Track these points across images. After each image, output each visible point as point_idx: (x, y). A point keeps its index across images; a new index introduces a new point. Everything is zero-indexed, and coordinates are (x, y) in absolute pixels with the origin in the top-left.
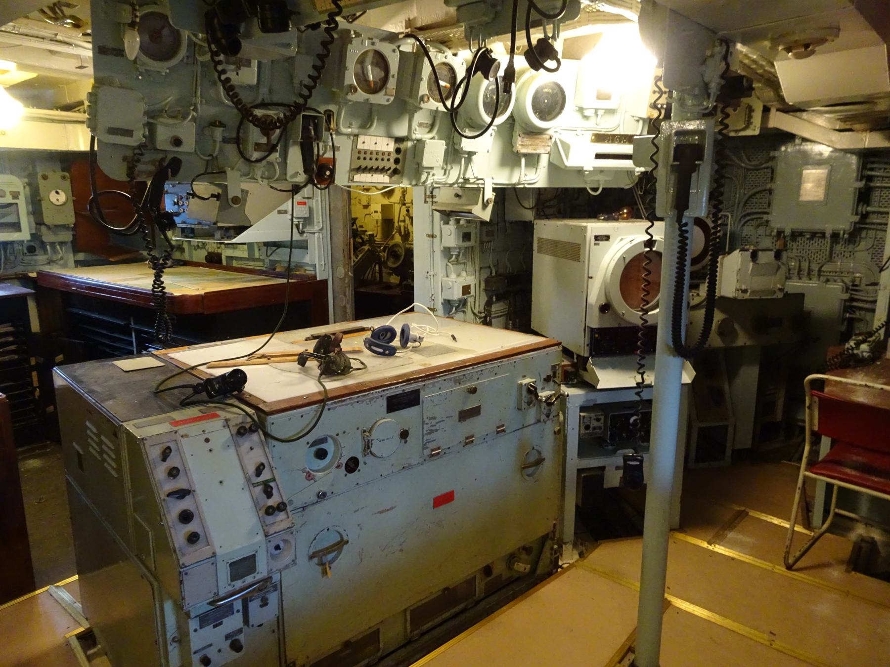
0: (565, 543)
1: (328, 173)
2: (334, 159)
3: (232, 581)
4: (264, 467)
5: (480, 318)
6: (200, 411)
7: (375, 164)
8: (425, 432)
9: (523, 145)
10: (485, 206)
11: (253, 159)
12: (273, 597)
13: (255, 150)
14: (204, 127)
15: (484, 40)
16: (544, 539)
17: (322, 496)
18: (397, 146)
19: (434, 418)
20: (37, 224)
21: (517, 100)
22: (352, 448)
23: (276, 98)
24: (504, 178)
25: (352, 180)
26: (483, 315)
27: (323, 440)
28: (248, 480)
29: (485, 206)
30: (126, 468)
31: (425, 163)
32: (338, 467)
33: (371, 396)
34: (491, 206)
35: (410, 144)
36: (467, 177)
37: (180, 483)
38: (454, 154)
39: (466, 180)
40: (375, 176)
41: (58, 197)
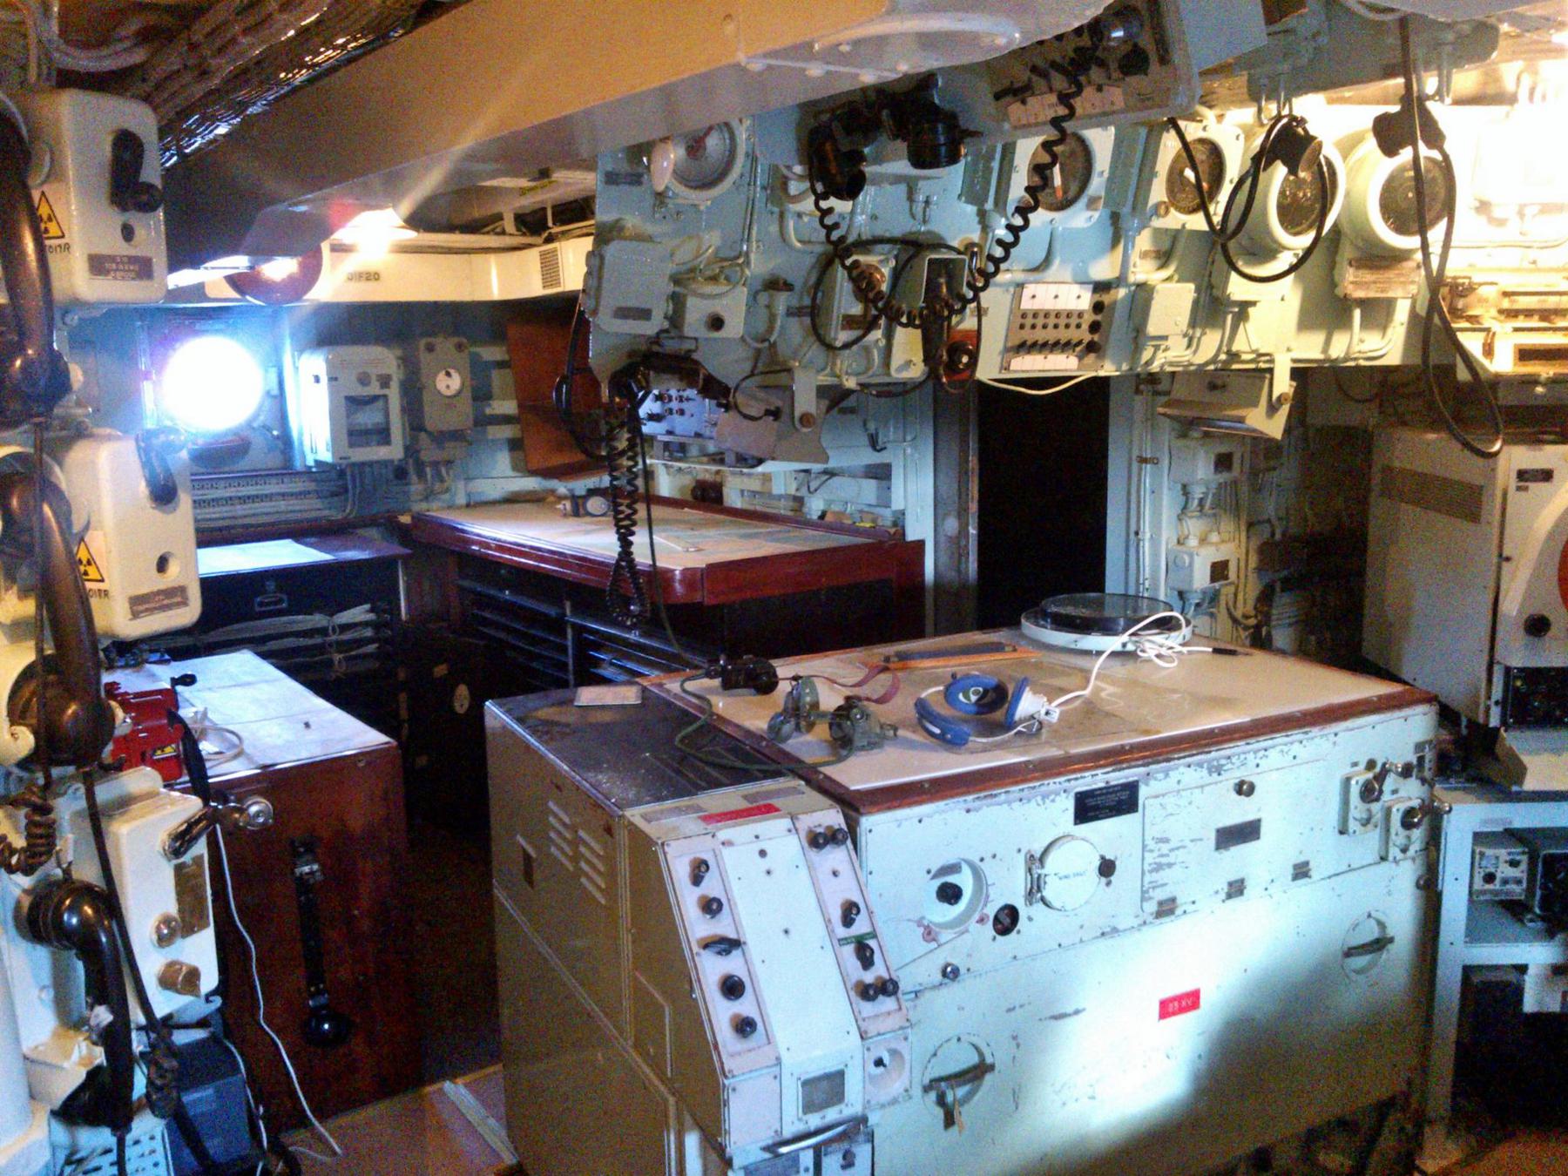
0: (1431, 1122)
1: (965, 359)
2: (979, 331)
3: (805, 1113)
4: (858, 912)
5: (1246, 628)
6: (745, 797)
7: (1050, 335)
8: (1147, 867)
9: (1354, 282)
10: (1273, 408)
11: (838, 344)
12: (862, 1152)
13: (843, 328)
14: (757, 293)
15: (1288, 100)
16: (1383, 1108)
17: (950, 973)
18: (1097, 297)
19: (1166, 840)
20: (413, 429)
21: (1347, 195)
22: (1009, 888)
23: (880, 230)
24: (1310, 348)
25: (1007, 369)
26: (1253, 622)
27: (953, 868)
28: (831, 932)
29: (1273, 408)
30: (625, 893)
31: (1152, 329)
32: (981, 920)
33: (1043, 789)
34: (1285, 410)
35: (1122, 293)
36: (1234, 348)
37: (721, 927)
38: (1213, 308)
39: (1234, 356)
40: (1051, 357)
41: (450, 382)
